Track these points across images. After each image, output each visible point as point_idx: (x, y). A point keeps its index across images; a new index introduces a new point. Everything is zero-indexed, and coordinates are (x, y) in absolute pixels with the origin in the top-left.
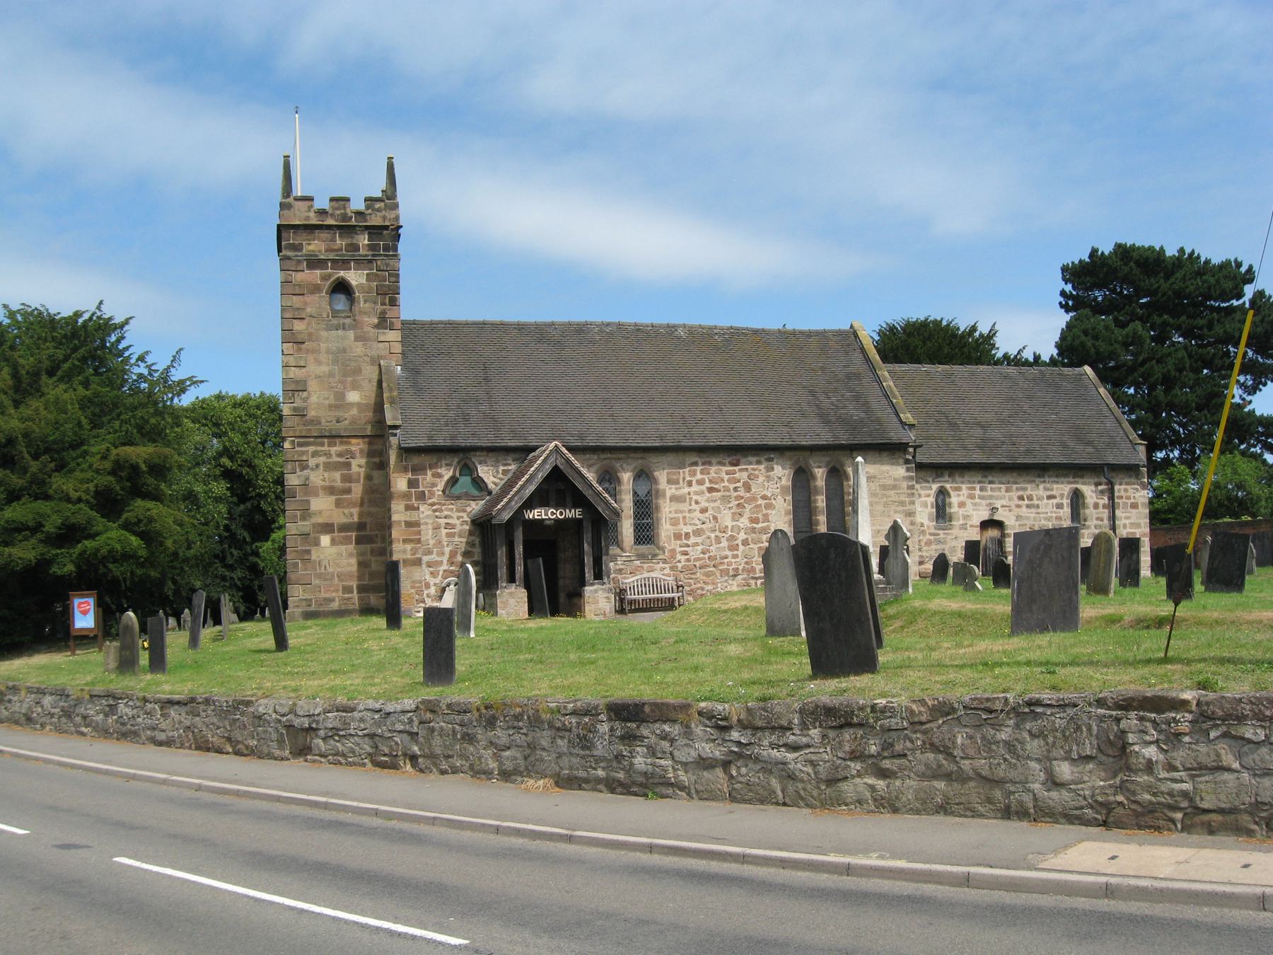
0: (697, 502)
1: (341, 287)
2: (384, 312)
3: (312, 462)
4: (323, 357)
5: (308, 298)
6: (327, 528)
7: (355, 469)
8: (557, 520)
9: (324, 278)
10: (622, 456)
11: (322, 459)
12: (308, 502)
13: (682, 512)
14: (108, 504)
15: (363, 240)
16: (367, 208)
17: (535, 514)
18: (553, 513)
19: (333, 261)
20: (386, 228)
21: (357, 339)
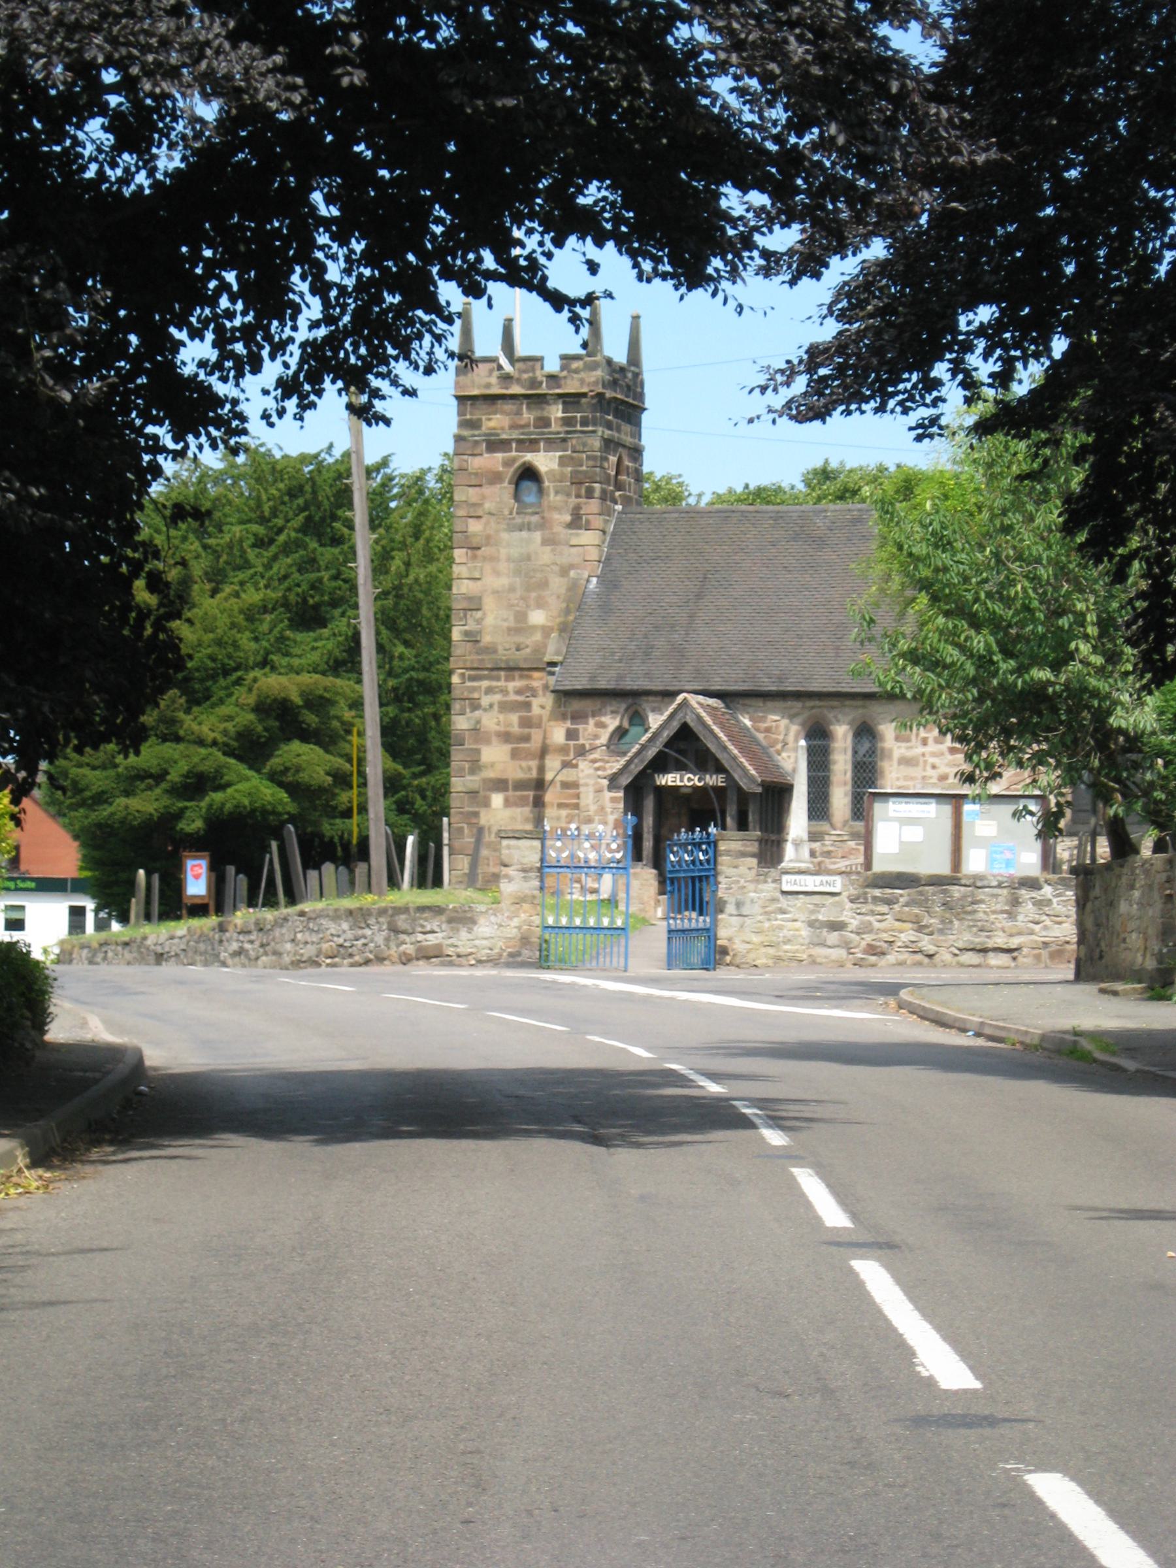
0: (934, 767)
1: (529, 474)
2: (577, 508)
3: (485, 701)
4: (503, 566)
5: (487, 490)
6: (500, 785)
7: (536, 710)
8: (694, 788)
9: (507, 463)
10: (835, 703)
11: (497, 698)
12: (478, 751)
13: (912, 779)
14: (251, 749)
15: (556, 412)
16: (563, 368)
17: (669, 779)
18: (689, 780)
19: (520, 442)
20: (584, 395)
21: (545, 542)
